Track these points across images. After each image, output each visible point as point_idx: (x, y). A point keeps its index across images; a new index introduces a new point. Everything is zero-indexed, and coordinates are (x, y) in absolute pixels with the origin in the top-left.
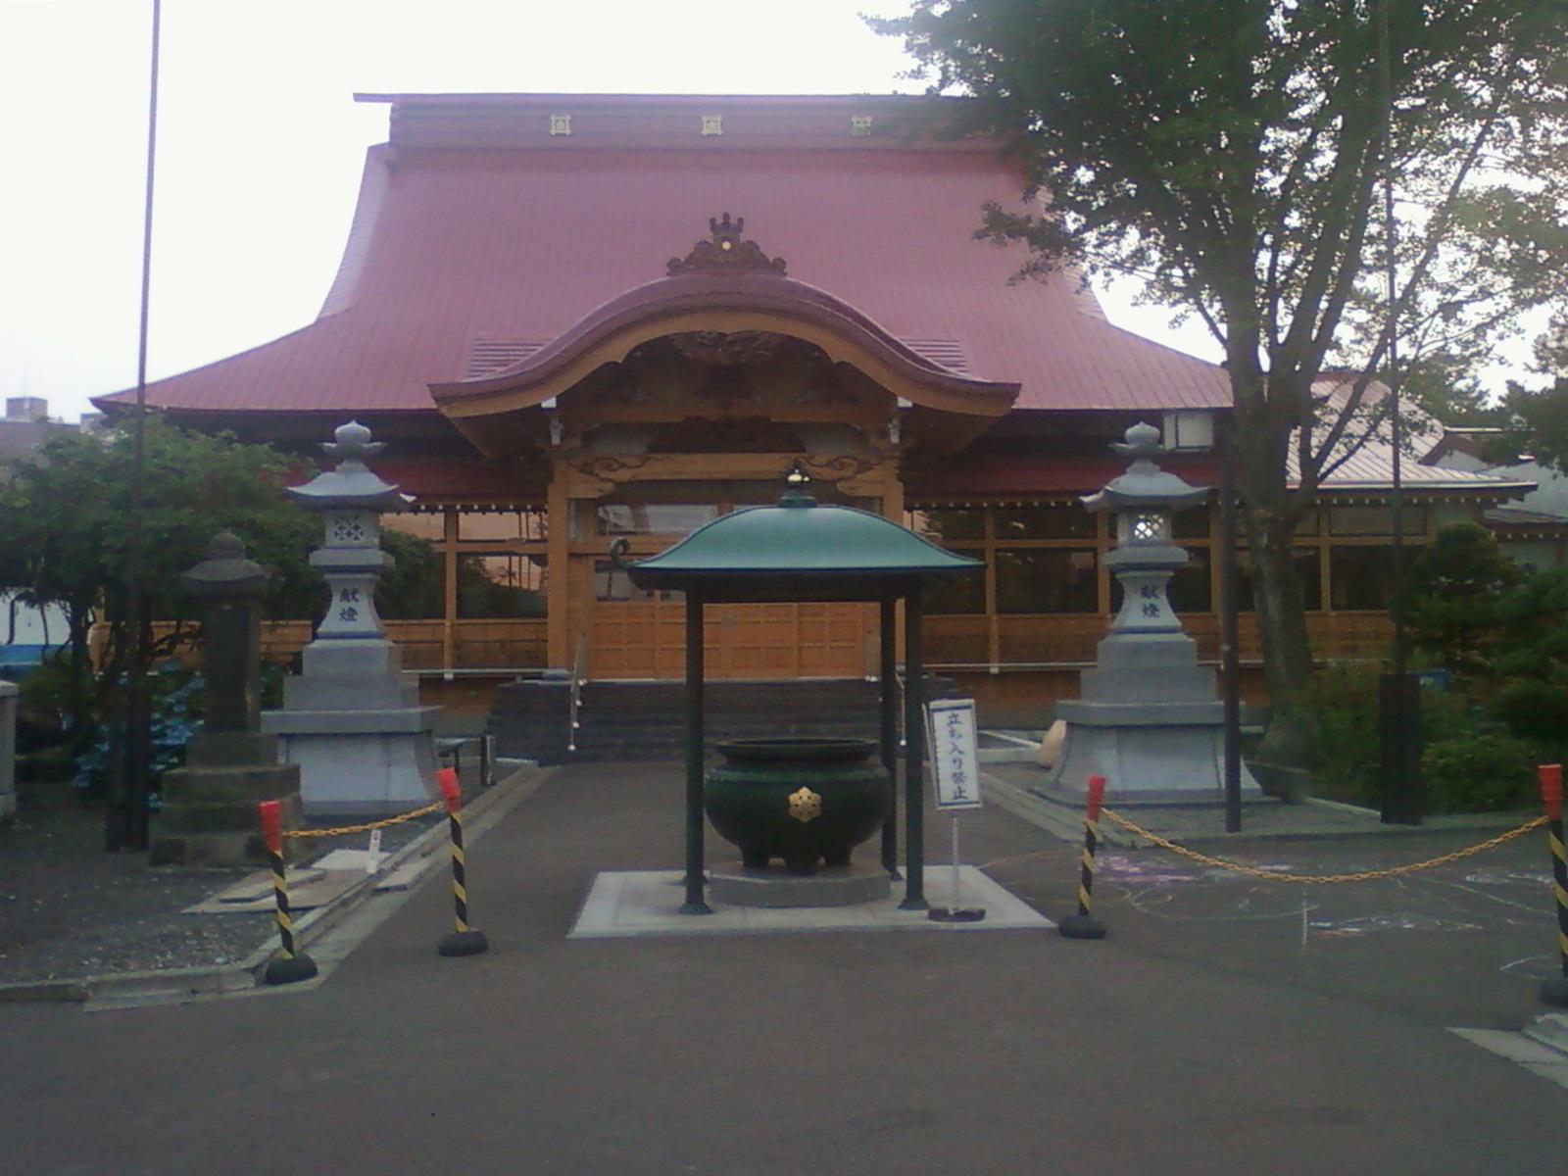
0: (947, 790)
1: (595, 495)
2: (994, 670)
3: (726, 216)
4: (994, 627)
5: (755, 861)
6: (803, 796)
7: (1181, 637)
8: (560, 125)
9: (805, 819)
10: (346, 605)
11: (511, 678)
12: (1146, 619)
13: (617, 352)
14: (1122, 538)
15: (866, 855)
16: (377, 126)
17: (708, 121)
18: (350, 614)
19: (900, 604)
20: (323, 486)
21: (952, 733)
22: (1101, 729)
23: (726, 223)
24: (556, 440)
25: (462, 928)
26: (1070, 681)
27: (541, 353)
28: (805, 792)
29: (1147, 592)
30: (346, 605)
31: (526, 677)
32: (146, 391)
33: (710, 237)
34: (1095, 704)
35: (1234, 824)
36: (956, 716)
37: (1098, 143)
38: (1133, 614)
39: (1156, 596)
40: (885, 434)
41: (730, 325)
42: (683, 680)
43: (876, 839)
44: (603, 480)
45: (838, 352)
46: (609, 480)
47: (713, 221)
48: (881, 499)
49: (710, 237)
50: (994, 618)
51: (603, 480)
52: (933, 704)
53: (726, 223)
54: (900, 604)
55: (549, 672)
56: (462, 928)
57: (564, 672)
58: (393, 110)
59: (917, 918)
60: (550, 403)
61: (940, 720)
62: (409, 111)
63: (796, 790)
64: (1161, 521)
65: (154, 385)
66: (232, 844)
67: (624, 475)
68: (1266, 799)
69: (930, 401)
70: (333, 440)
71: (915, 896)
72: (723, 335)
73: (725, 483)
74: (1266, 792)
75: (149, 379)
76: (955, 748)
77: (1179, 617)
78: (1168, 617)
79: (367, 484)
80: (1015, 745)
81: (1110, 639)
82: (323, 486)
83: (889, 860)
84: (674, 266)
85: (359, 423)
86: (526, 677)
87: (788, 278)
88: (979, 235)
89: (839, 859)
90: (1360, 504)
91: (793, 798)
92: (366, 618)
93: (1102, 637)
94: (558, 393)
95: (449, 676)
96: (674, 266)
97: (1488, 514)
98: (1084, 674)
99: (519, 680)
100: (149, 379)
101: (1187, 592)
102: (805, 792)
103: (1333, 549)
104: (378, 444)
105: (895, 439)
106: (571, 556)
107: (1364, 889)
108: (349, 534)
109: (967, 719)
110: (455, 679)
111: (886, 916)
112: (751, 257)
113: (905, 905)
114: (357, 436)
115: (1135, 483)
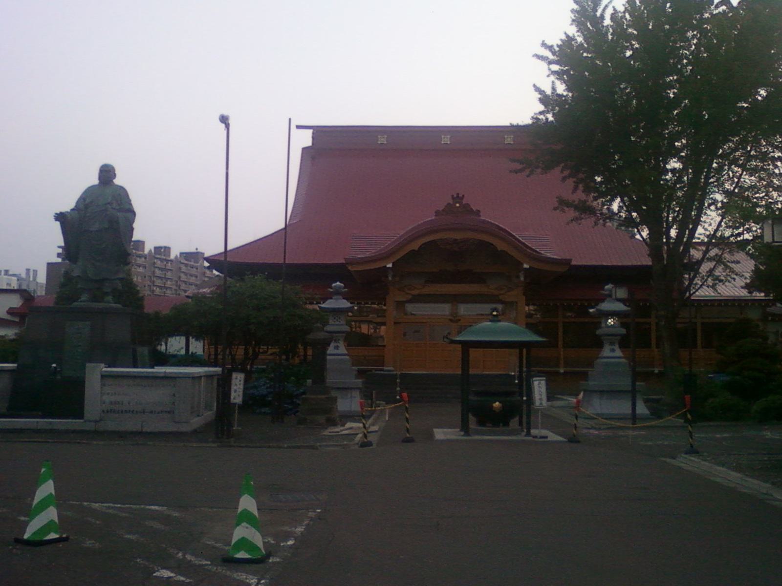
0: (537, 403)
1: (405, 300)
2: (562, 371)
3: (458, 194)
4: (562, 353)
5: (481, 422)
6: (497, 404)
7: (623, 360)
8: (382, 140)
9: (497, 411)
10: (336, 344)
11: (371, 370)
12: (611, 353)
13: (415, 246)
14: (603, 325)
15: (514, 423)
16: (305, 139)
17: (444, 138)
18: (337, 348)
19: (525, 350)
20: (328, 304)
21: (539, 387)
22: (596, 391)
23: (458, 197)
24: (390, 278)
25: (408, 435)
26: (584, 376)
27: (387, 246)
28: (497, 403)
29: (612, 343)
30: (336, 344)
31: (376, 370)
32: (228, 253)
33: (451, 202)
34: (592, 383)
35: (634, 423)
36: (540, 382)
37: (611, 145)
38: (606, 352)
39: (615, 346)
40: (518, 277)
41: (459, 236)
42: (460, 372)
43: (517, 419)
44: (407, 294)
45: (500, 246)
46: (410, 294)
47: (453, 196)
48: (517, 303)
49: (451, 202)
50: (562, 350)
51: (407, 294)
52: (534, 379)
53: (458, 197)
54: (525, 350)
55: (386, 368)
56: (408, 435)
57: (391, 368)
58: (313, 133)
59: (530, 438)
60: (390, 265)
61: (536, 383)
62: (321, 133)
63: (495, 403)
64: (617, 319)
65: (230, 250)
66: (321, 419)
67: (416, 292)
68: (651, 417)
69: (536, 265)
70: (331, 288)
71: (528, 434)
72: (456, 240)
73: (455, 296)
74: (652, 414)
75: (229, 248)
76: (540, 391)
77: (622, 351)
78: (618, 353)
79: (344, 304)
80: (566, 400)
81: (598, 360)
82: (328, 304)
83: (521, 423)
84: (437, 213)
85: (340, 282)
86: (376, 370)
87: (482, 218)
88: (555, 209)
89: (506, 424)
90: (719, 305)
91: (494, 405)
92: (343, 350)
93: (597, 358)
94: (393, 261)
95: (562, 371)
96: (437, 213)
97: (768, 309)
98: (590, 373)
99: (374, 371)
100: (229, 248)
101: (624, 343)
102: (497, 403)
103: (703, 324)
104: (346, 290)
105: (522, 279)
106: (395, 323)
107: (716, 465)
108: (337, 320)
109: (543, 383)
110: (564, 372)
111: (521, 437)
112: (467, 209)
113: (526, 436)
114: (340, 287)
115: (606, 306)
